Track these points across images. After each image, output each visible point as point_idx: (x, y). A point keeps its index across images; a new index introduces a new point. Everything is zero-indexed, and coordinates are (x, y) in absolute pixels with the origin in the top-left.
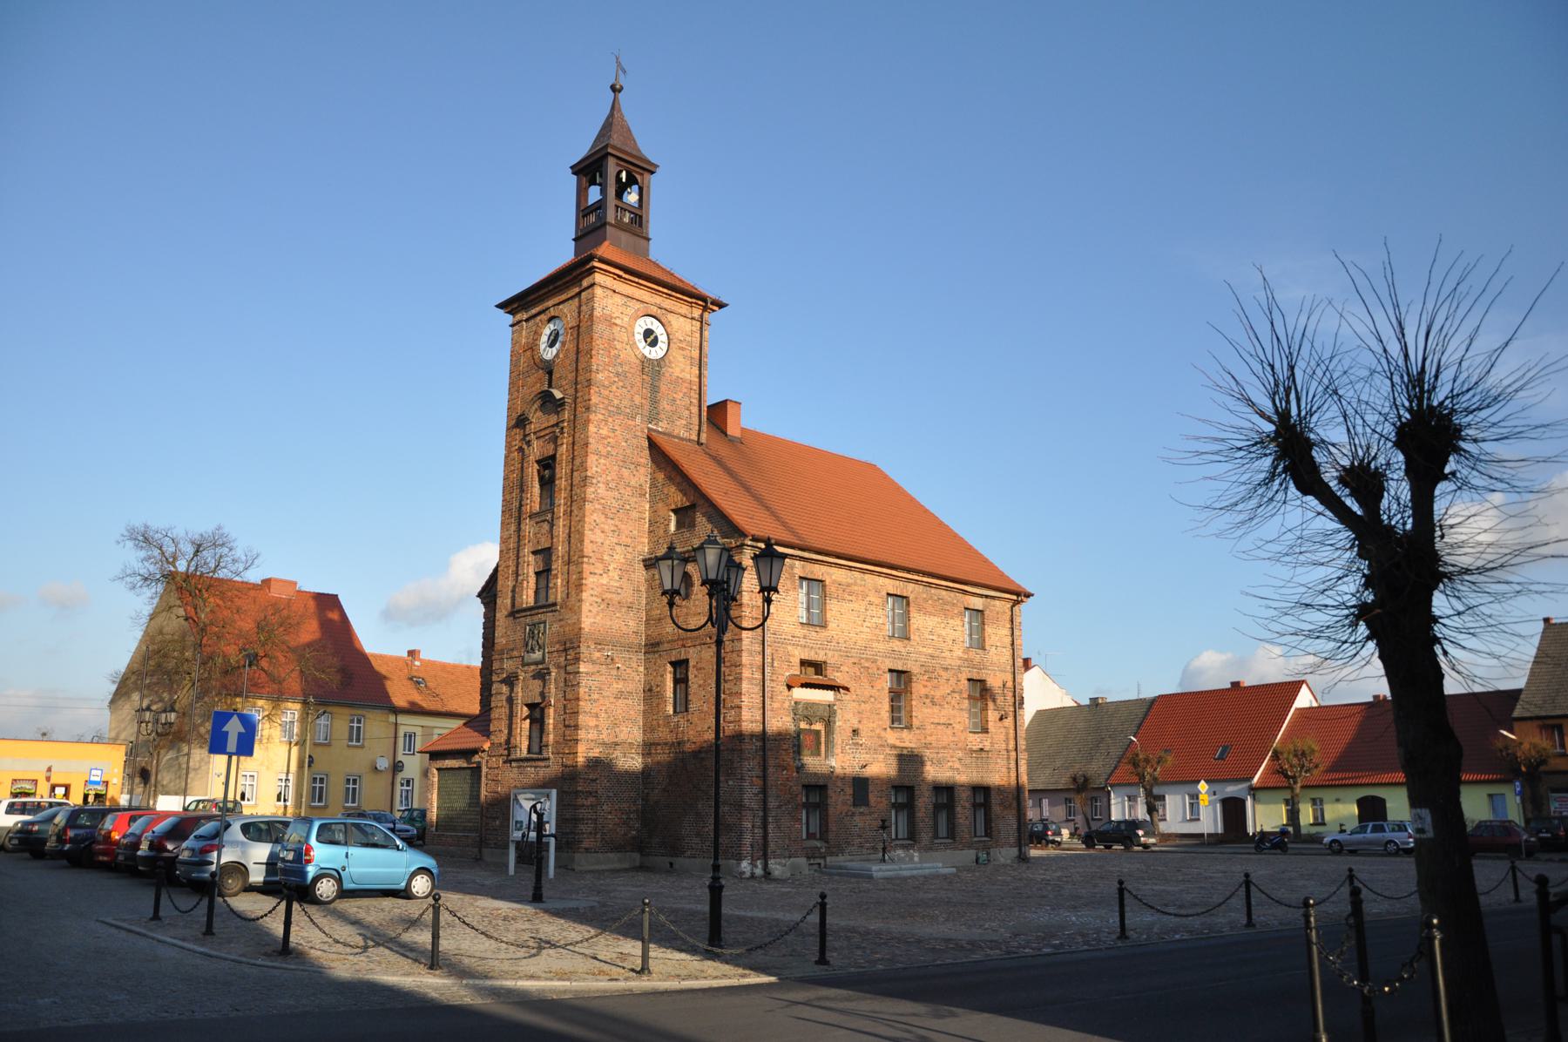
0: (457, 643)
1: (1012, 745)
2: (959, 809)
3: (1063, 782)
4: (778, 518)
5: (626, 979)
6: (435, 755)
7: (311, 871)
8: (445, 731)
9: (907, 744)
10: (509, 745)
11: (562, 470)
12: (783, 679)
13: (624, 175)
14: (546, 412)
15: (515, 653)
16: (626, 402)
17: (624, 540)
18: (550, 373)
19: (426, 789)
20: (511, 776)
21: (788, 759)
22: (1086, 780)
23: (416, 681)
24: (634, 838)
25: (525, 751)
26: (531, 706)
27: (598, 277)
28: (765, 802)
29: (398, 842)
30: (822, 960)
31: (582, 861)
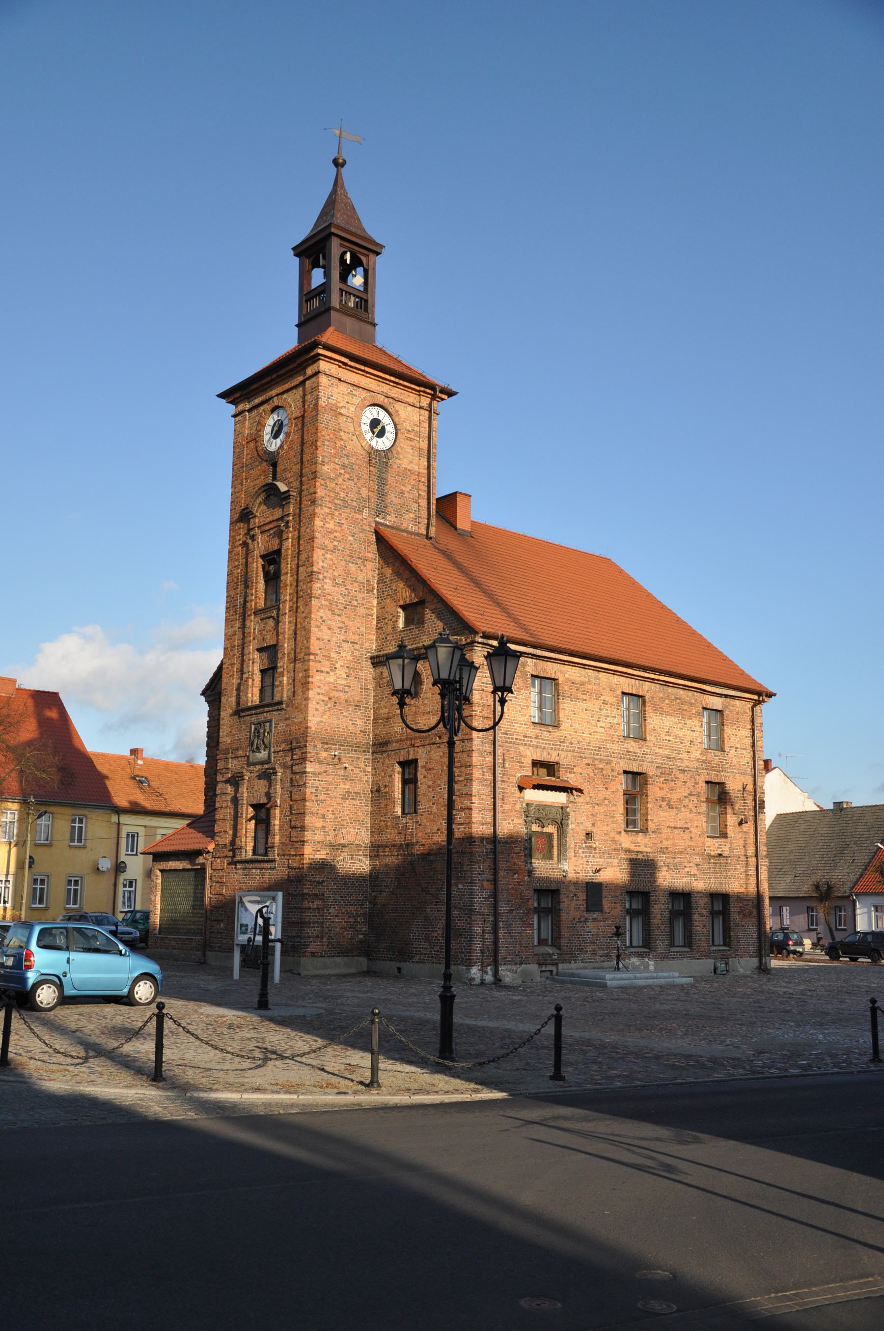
0: (178, 736)
1: (751, 851)
2: (696, 917)
3: (805, 889)
4: (509, 615)
5: (355, 1093)
6: (158, 857)
7: (32, 977)
8: (170, 832)
9: (642, 849)
10: (234, 847)
11: (287, 566)
12: (514, 780)
13: (348, 256)
14: (270, 509)
15: (241, 753)
16: (352, 495)
17: (351, 637)
18: (274, 465)
19: (149, 890)
20: (236, 878)
21: (520, 863)
22: (830, 888)
23: (139, 781)
24: (361, 942)
25: (250, 852)
26: (256, 807)
27: (323, 365)
28: (495, 906)
29: (121, 947)
30: (557, 1076)
31: (309, 965)
